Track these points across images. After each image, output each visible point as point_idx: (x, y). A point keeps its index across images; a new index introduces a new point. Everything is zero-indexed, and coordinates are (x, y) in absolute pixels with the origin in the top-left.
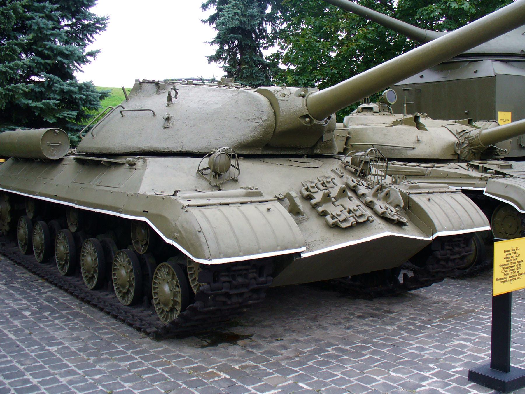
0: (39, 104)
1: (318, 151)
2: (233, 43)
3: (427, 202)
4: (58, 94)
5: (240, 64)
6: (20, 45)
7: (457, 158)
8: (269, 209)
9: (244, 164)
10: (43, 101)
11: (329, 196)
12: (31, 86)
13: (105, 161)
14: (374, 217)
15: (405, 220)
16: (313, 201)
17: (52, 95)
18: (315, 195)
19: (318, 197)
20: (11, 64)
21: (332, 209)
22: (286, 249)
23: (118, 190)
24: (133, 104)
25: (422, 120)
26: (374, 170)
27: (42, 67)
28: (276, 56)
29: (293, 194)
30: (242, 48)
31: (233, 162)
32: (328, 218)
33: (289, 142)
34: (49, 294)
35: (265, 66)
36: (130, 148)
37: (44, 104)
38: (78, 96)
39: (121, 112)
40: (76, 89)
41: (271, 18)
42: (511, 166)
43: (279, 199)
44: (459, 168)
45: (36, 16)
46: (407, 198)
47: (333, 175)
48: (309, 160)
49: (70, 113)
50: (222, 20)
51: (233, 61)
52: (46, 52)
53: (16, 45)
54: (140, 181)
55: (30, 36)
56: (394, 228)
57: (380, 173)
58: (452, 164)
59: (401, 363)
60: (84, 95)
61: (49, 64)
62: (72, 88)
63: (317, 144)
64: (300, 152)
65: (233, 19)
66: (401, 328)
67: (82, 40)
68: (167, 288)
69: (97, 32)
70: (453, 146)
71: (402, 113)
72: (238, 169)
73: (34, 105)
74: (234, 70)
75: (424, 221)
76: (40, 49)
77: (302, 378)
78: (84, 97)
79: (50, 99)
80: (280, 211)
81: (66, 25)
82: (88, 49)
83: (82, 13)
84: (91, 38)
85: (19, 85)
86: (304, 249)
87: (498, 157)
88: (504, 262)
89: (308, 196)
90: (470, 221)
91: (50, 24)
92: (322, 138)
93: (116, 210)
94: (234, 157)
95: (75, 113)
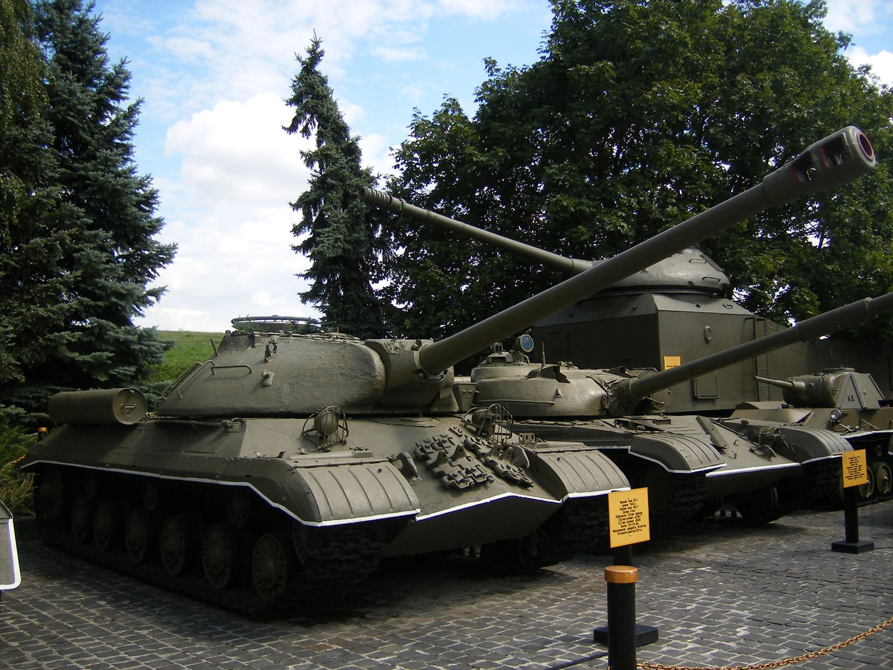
0: (87, 358)
1: (436, 410)
2: (334, 276)
3: (557, 462)
4: (112, 345)
5: (344, 303)
6: (65, 283)
7: (605, 413)
8: (380, 470)
9: (352, 425)
10: (93, 354)
11: (444, 456)
12: (78, 334)
13: (196, 425)
14: (494, 477)
15: (530, 480)
16: (430, 462)
17: (104, 347)
18: (430, 455)
19: (434, 457)
20: (55, 308)
21: (445, 468)
22: (400, 511)
23: (214, 455)
24: (224, 359)
25: (563, 371)
26: (497, 429)
27: (92, 310)
28: (390, 291)
29: (407, 455)
30: (345, 283)
31: (341, 423)
32: (445, 478)
33: (396, 401)
34: (122, 584)
35: (376, 305)
36: (224, 409)
37: (93, 357)
38: (137, 347)
39: (212, 368)
40: (135, 338)
41: (382, 244)
42: (669, 422)
43: (391, 461)
44: (607, 425)
45: (86, 247)
46: (533, 456)
47: (450, 435)
48: (426, 419)
49: (126, 368)
50: (319, 248)
51: (334, 299)
52: (98, 292)
53: (61, 283)
54: (239, 444)
55: (79, 273)
56: (517, 488)
57: (504, 431)
58: (600, 422)
59: (525, 631)
60: (144, 345)
61: (100, 307)
62: (130, 337)
63: (433, 400)
64: (415, 411)
65: (334, 247)
66: (531, 601)
67: (141, 274)
68: (271, 565)
69: (160, 266)
70: (602, 399)
71: (541, 362)
72: (346, 430)
73: (81, 359)
74: (336, 310)
75: (553, 484)
76: (90, 288)
77: (418, 646)
78: (145, 348)
79: (104, 351)
80: (392, 475)
81: (120, 257)
82: (149, 286)
83: (142, 241)
84: (153, 273)
85: (63, 333)
86: (418, 511)
87: (655, 412)
88: (621, 513)
89: (423, 456)
90: (606, 481)
91: (104, 256)
92: (439, 394)
93: (212, 476)
94: (341, 417)
95: (133, 369)
